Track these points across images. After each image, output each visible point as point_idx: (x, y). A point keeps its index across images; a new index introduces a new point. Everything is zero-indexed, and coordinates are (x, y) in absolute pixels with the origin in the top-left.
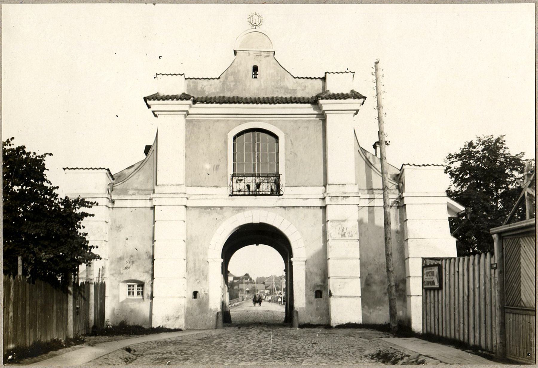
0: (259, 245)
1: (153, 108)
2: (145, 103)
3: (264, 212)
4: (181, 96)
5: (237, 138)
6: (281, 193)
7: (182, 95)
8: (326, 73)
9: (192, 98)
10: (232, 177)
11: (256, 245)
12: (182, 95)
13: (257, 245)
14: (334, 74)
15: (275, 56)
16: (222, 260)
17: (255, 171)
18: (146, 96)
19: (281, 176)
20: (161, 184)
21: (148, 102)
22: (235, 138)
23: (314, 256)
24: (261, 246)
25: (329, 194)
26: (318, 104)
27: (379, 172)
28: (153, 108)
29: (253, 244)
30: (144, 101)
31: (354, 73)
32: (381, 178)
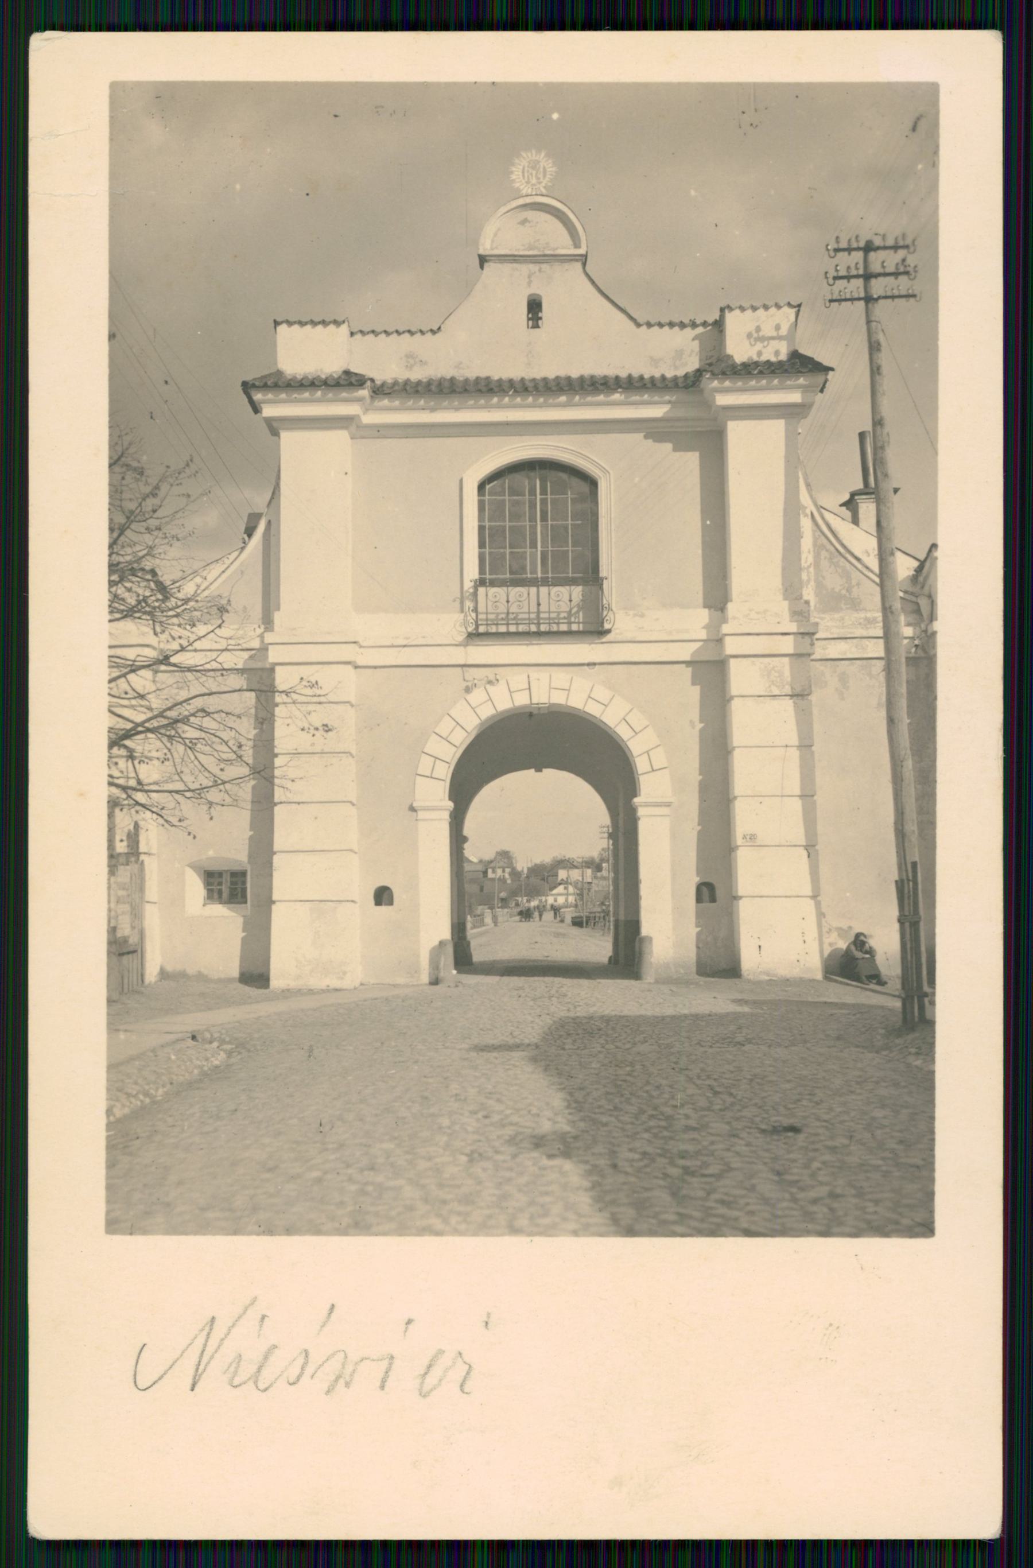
0: (545, 771)
1: (269, 411)
2: (246, 400)
3: (561, 677)
4: (340, 377)
5: (488, 487)
6: (607, 626)
7: (343, 377)
8: (722, 310)
9: (369, 383)
10: (476, 588)
11: (536, 771)
12: (343, 377)
13: (539, 770)
14: (407, 329)
15: (587, 268)
16: (451, 805)
17: (536, 573)
18: (248, 378)
19: (605, 581)
20: (856, 303)
21: (258, 396)
22: (481, 487)
23: (586, 1162)
24: (548, 772)
25: (857, 264)
26: (702, 391)
27: (872, 572)
28: (269, 411)
29: (528, 768)
30: (242, 392)
31: (799, 306)
32: (878, 589)
